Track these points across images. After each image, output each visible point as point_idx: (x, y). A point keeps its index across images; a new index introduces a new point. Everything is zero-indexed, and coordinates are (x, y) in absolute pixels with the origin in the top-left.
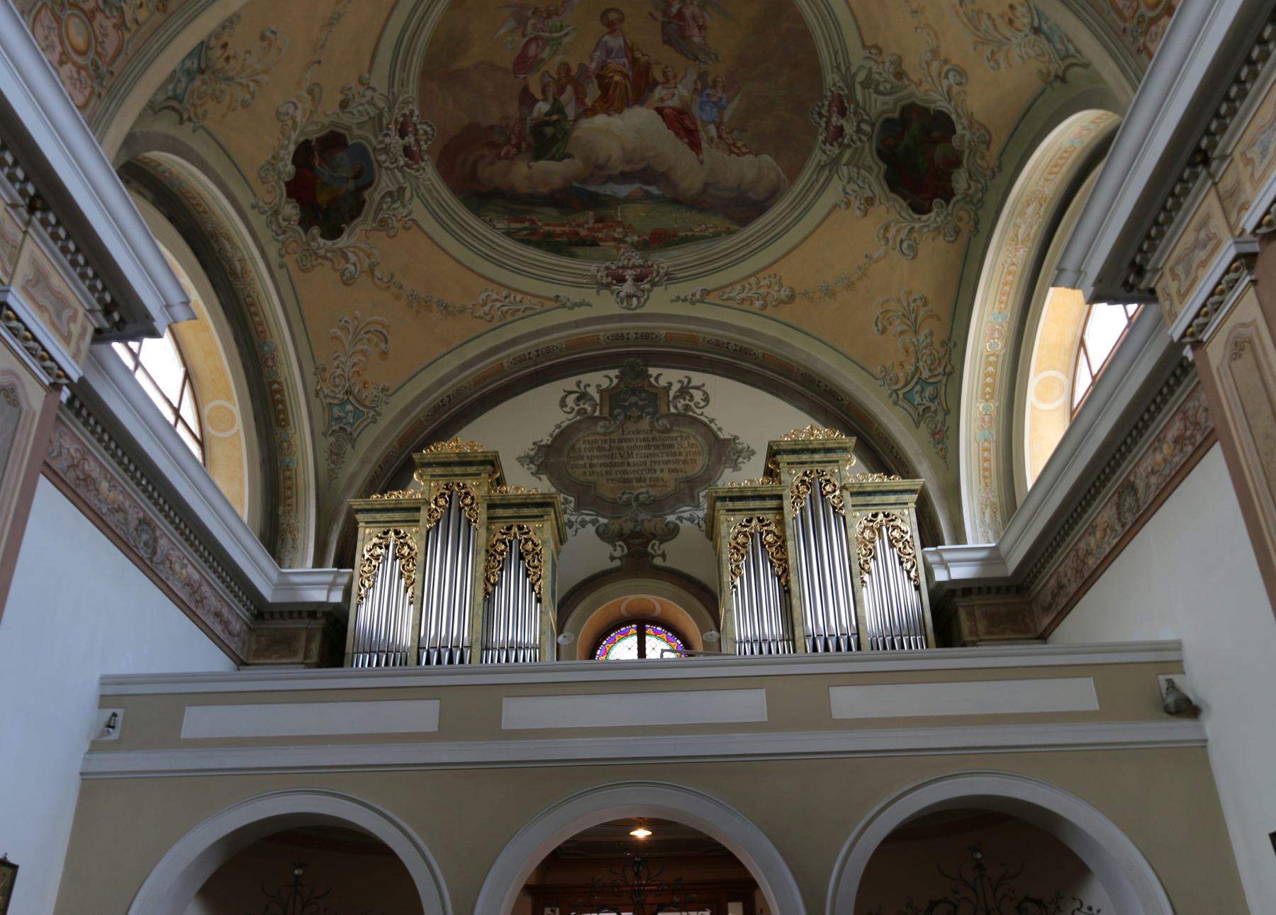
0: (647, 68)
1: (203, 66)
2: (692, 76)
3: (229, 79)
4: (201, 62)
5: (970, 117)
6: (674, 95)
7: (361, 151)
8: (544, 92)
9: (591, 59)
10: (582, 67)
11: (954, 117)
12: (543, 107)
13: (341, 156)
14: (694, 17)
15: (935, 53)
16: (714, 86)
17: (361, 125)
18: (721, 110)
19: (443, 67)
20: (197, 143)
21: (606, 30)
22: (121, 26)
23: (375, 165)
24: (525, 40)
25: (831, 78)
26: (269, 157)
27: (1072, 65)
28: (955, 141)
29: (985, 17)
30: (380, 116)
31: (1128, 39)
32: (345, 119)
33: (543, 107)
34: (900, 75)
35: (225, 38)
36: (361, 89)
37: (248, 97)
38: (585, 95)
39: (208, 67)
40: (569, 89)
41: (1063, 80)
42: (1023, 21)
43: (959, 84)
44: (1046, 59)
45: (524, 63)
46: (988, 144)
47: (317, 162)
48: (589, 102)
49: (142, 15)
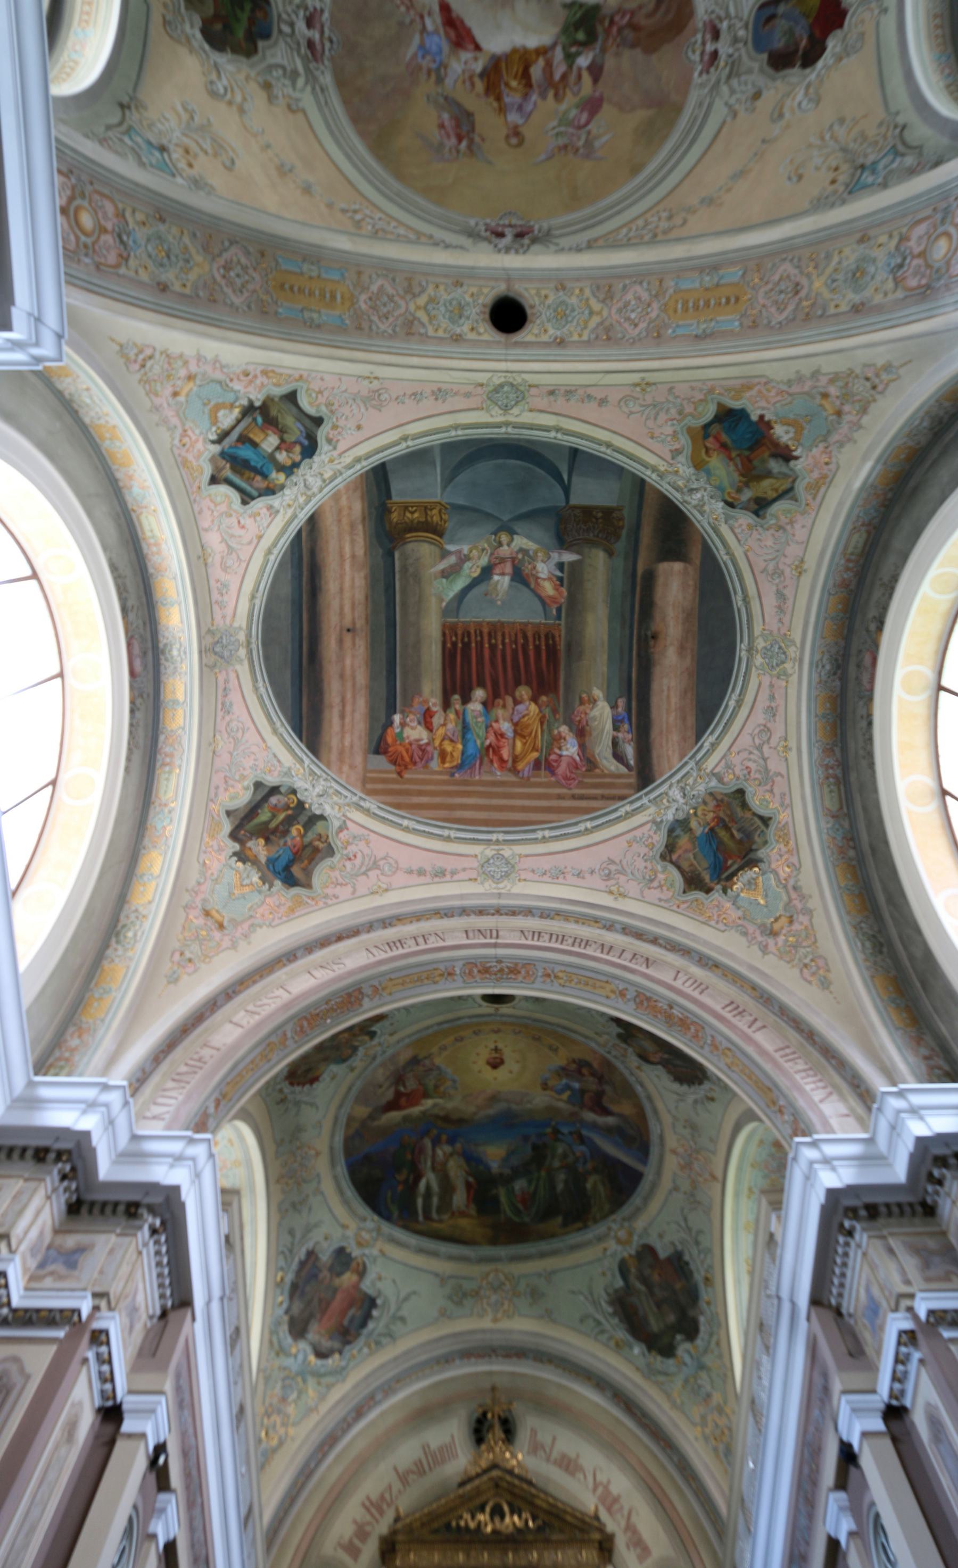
0: (488, 91)
1: (859, 172)
2: (449, 81)
3: (844, 150)
4: (859, 175)
5: (191, 50)
6: (466, 63)
7: (759, 43)
8: (579, 77)
9: (535, 104)
10: (543, 96)
11: (207, 47)
12: (583, 61)
13: (779, 42)
14: (448, 136)
15: (242, 111)
16: (429, 72)
17: (750, 71)
18: (422, 46)
19: (663, 111)
20: (901, 98)
21: (521, 129)
22: (903, 239)
23: (751, 26)
24: (589, 127)
25: (327, 79)
26: (845, 61)
27: (120, 124)
28: (198, 22)
29: (210, 151)
30: (729, 77)
31: (84, 177)
32: (761, 81)
33: (583, 61)
34: (267, 86)
35: (831, 188)
36: (737, 107)
37: (836, 128)
38: (544, 70)
39: (856, 169)
40: (557, 76)
41: (123, 107)
42: (177, 154)
43: (212, 82)
44: (145, 123)
45: (593, 106)
46: (166, 22)
47: (804, 43)
48: (541, 62)
49: (883, 239)
